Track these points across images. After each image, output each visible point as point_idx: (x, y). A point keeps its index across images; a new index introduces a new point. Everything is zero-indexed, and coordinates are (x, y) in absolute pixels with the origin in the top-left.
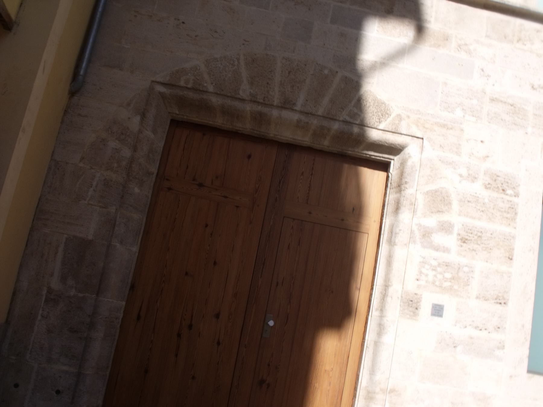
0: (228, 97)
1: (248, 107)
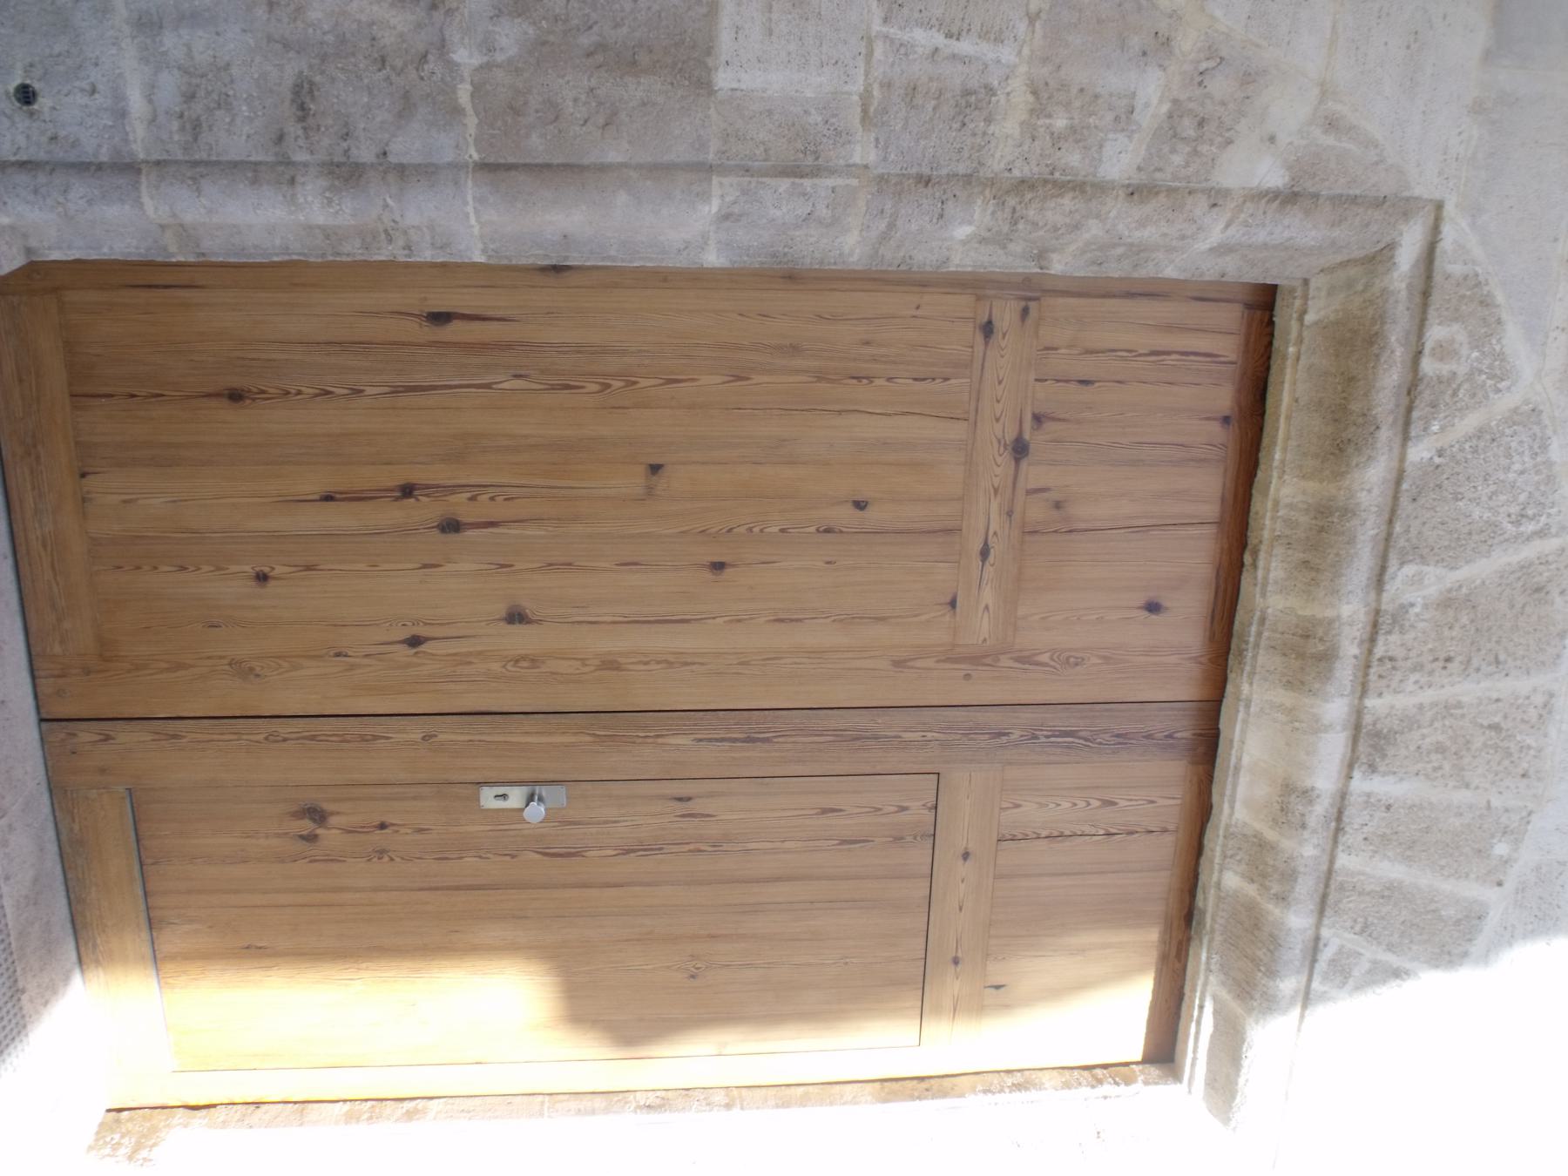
0: (1390, 522)
1: (1351, 610)
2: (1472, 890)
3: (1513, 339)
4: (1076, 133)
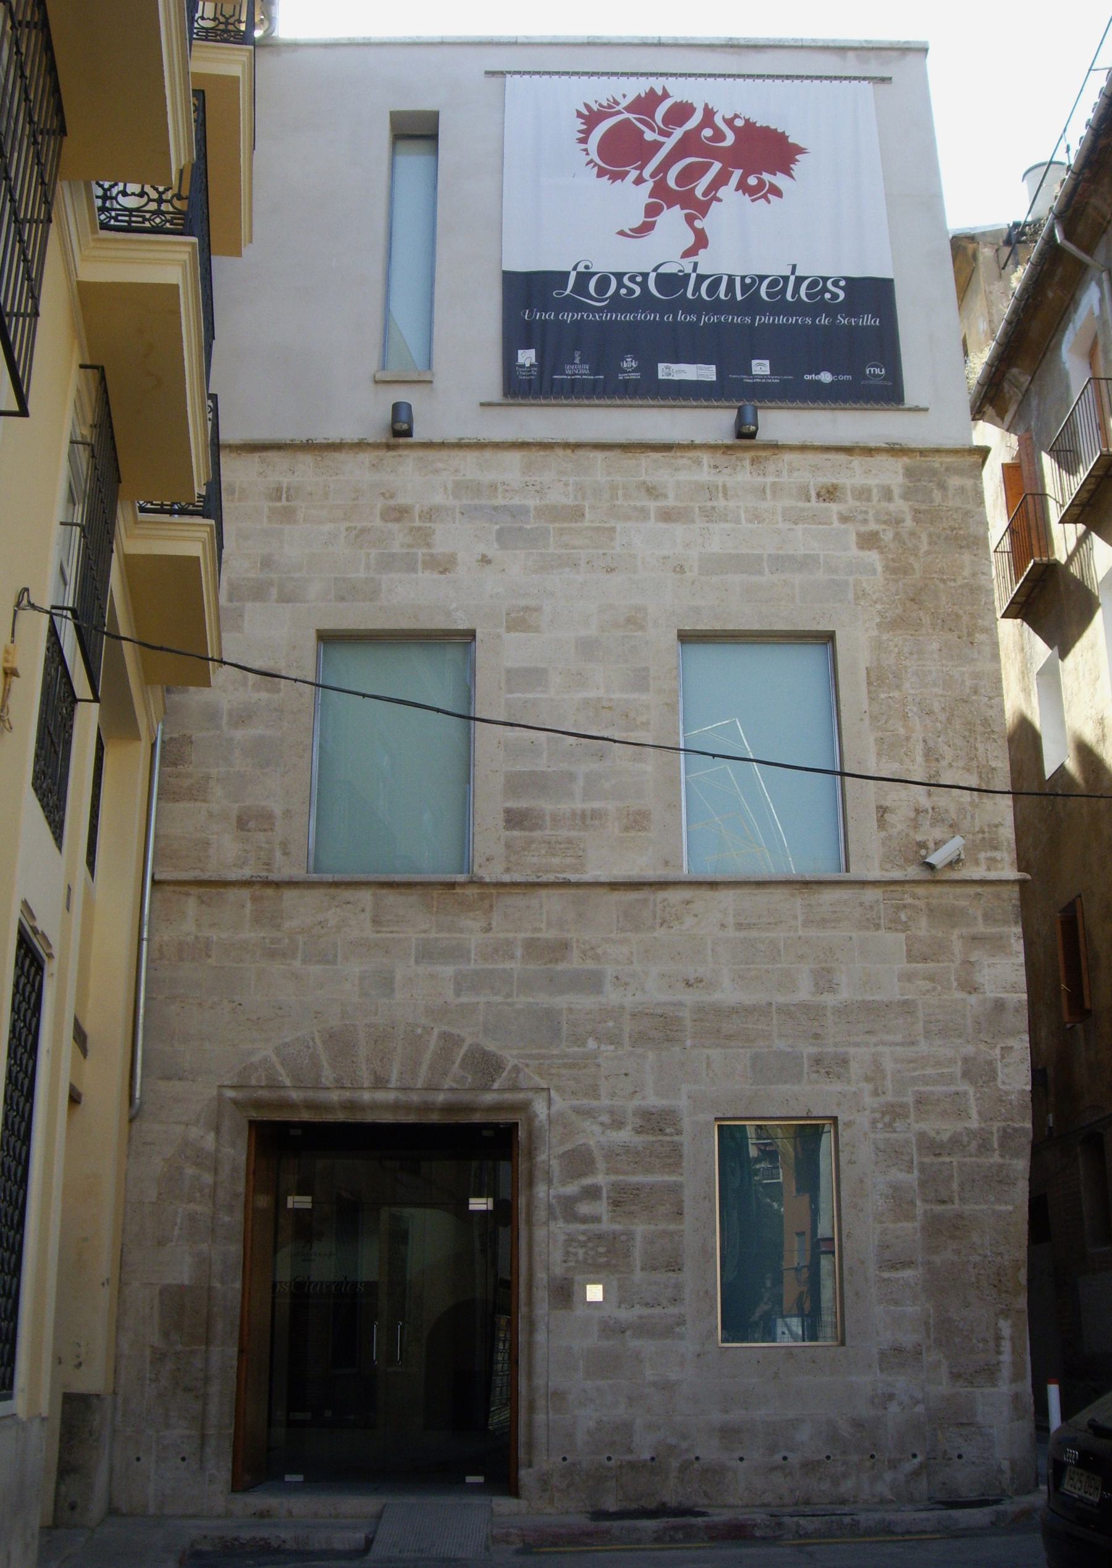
3: (255, 1059)
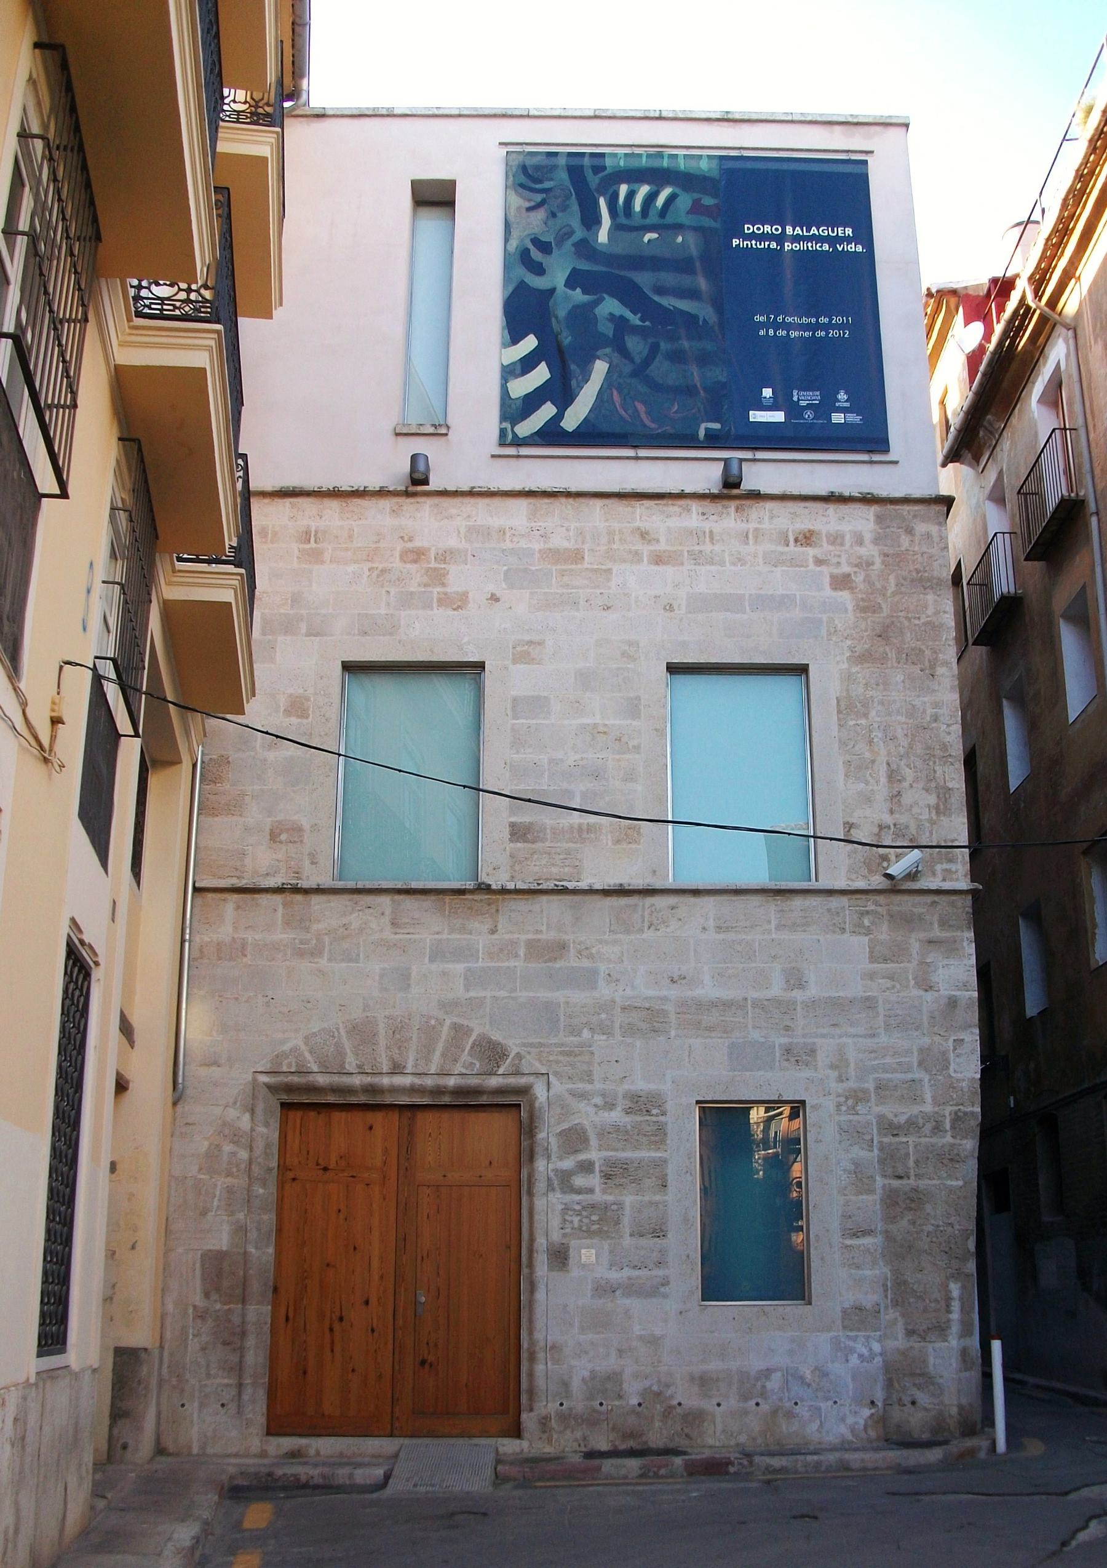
2: (445, 1030)
3: (286, 1047)
4: (237, 1166)
